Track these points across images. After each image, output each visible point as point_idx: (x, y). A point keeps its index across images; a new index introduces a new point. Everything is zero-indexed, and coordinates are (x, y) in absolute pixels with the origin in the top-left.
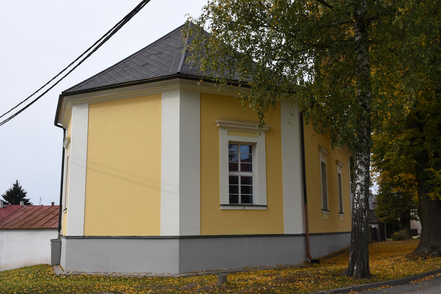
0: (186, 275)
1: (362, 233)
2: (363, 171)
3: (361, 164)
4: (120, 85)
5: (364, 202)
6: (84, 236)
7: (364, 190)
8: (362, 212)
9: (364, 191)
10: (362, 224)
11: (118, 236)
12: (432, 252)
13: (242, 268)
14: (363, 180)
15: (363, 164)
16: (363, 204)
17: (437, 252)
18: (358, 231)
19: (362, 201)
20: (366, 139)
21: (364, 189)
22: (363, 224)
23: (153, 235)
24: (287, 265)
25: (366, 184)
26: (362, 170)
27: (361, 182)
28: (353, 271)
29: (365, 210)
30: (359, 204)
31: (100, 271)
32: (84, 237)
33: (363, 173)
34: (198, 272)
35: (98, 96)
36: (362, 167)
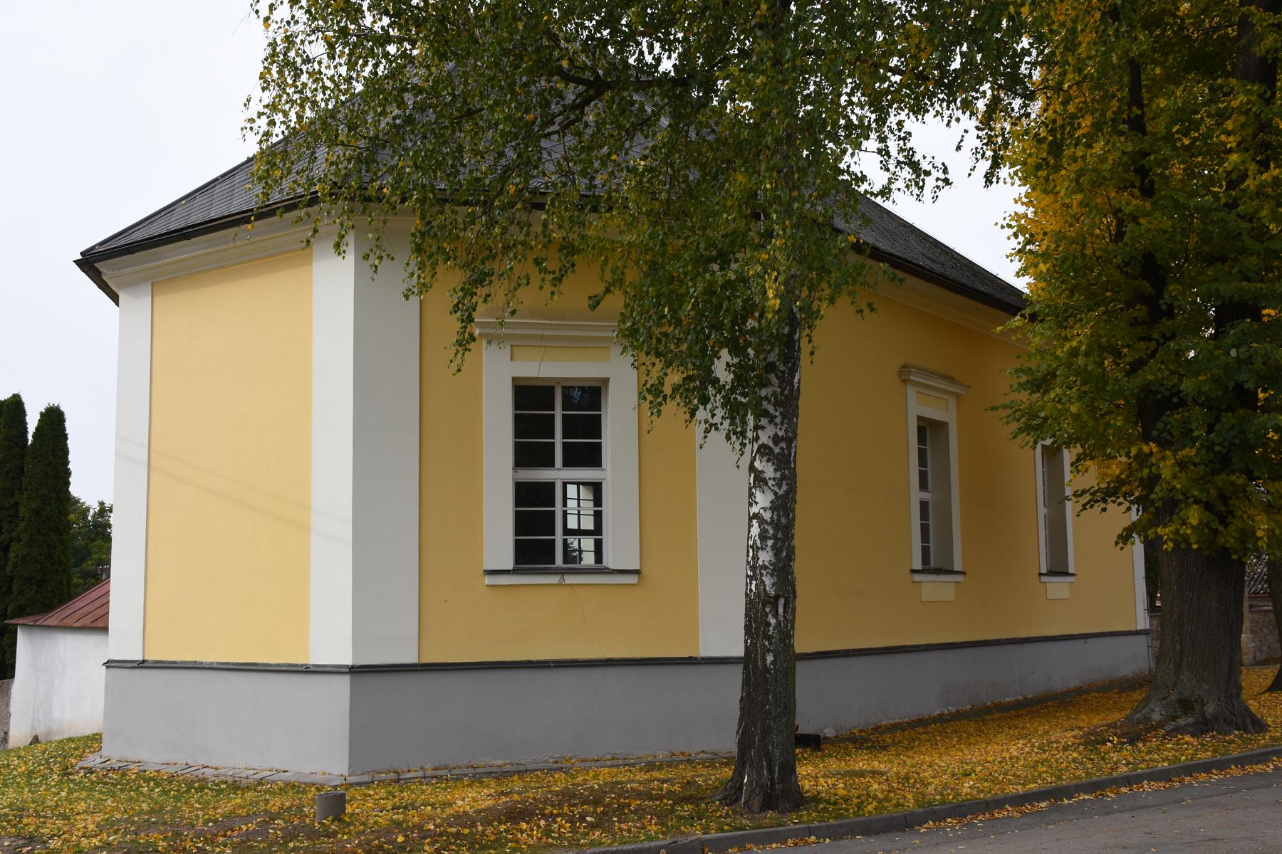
0: (366, 778)
1: (767, 670)
2: (767, 478)
3: (762, 455)
4: (221, 221)
5: (772, 575)
6: (144, 661)
7: (770, 535)
8: (764, 606)
9: (770, 538)
10: (767, 643)
11: (218, 663)
12: (1174, 719)
13: (551, 760)
14: (768, 505)
15: (767, 454)
16: (768, 581)
17: (1191, 720)
18: (756, 666)
19: (764, 572)
20: (780, 375)
21: (771, 532)
22: (770, 644)
23: (294, 662)
24: (703, 752)
25: (779, 516)
26: (764, 472)
27: (762, 511)
28: (740, 789)
29: (777, 598)
30: (756, 580)
31: (174, 761)
32: (142, 665)
33: (766, 484)
34: (409, 771)
35: (165, 261)
36: (764, 463)
